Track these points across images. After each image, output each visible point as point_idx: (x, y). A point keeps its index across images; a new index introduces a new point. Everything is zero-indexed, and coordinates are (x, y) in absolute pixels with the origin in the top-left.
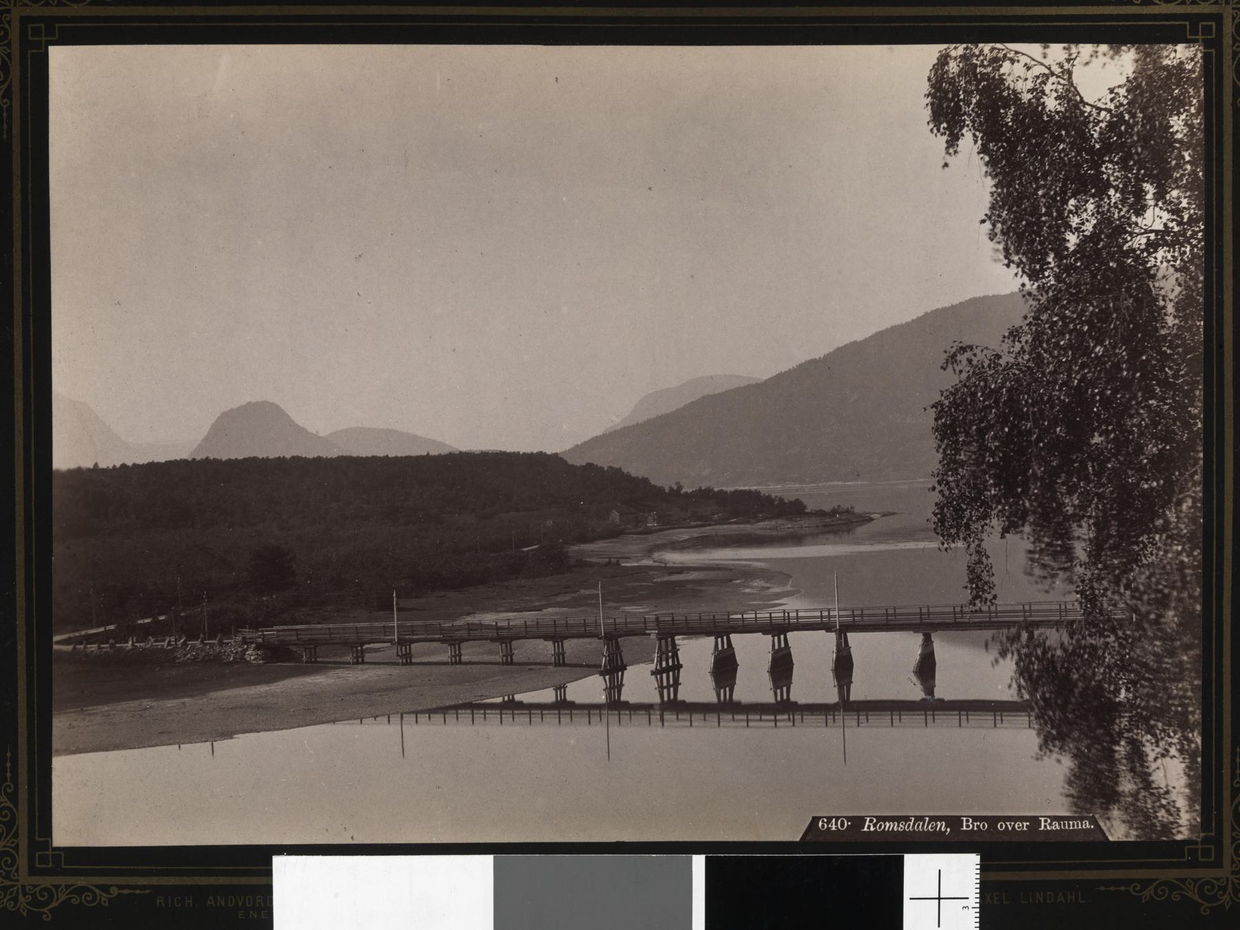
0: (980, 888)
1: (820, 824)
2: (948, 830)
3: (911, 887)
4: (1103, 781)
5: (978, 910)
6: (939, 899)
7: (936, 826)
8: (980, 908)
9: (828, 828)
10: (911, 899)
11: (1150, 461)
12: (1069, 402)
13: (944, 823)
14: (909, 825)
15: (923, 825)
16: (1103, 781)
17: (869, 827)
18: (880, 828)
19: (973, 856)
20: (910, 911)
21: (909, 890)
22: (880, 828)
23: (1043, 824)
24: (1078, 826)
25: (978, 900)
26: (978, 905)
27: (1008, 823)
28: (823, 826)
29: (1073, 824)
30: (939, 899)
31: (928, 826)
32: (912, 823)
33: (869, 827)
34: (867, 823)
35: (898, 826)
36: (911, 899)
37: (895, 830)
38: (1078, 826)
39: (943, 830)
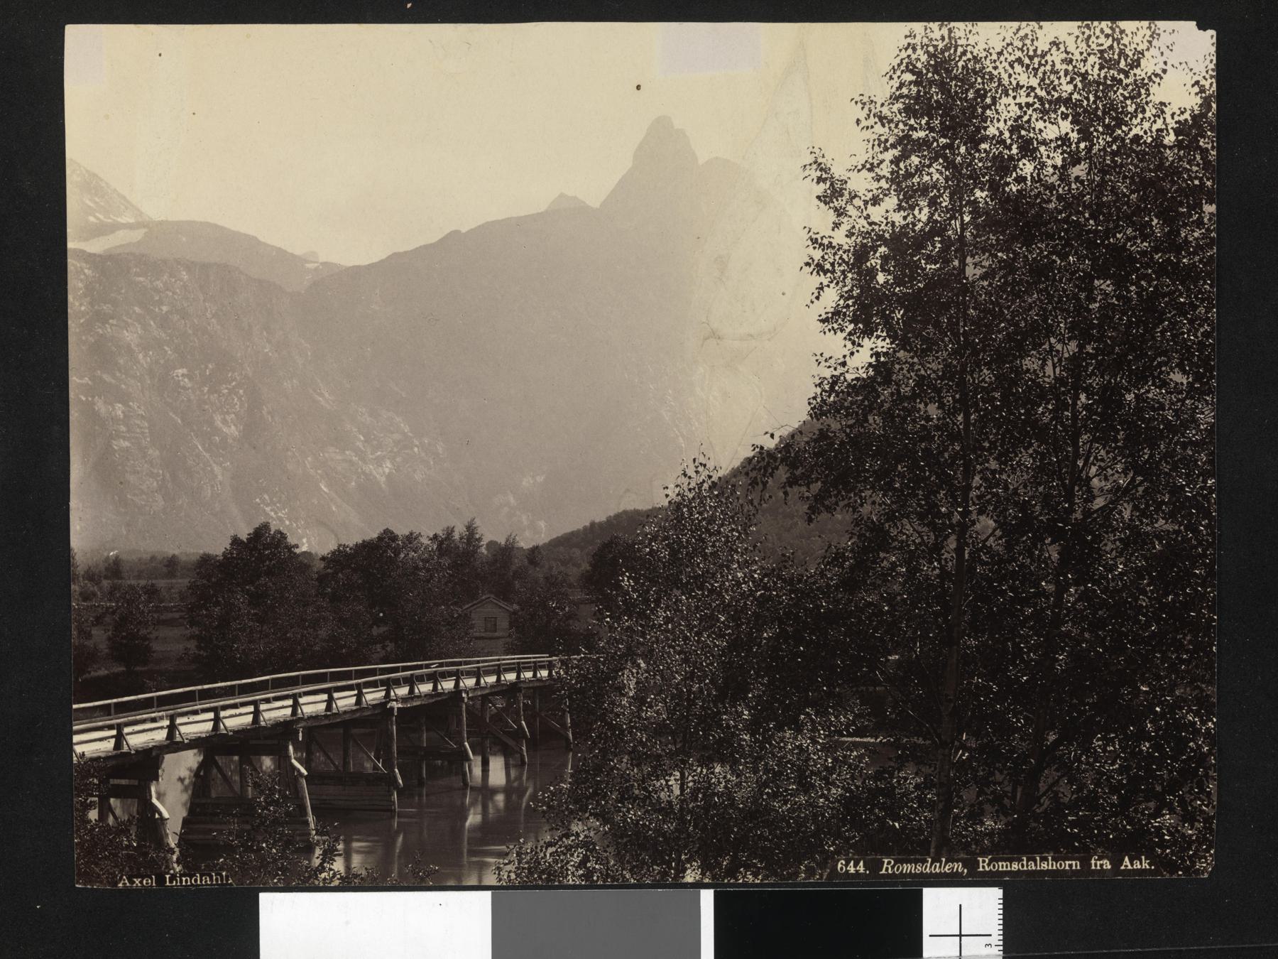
0: (1003, 925)
1: (839, 866)
2: (966, 871)
3: (930, 923)
4: (711, 752)
5: (1001, 948)
6: (960, 936)
7: (953, 868)
8: (1003, 945)
9: (847, 871)
10: (930, 936)
11: (895, 480)
12: (850, 493)
13: (960, 864)
14: (926, 867)
15: (940, 867)
16: (711, 752)
17: (887, 869)
18: (898, 870)
19: (996, 889)
20: (930, 947)
21: (928, 926)
22: (898, 870)
23: (981, 864)
24: (1007, 867)
25: (1001, 937)
26: (1001, 943)
27: (1130, 867)
28: (842, 869)
29: (1003, 865)
30: (960, 936)
31: (944, 867)
32: (929, 865)
33: (887, 869)
34: (885, 866)
35: (916, 868)
36: (930, 936)
37: (913, 872)
38: (1007, 867)
39: (960, 871)
